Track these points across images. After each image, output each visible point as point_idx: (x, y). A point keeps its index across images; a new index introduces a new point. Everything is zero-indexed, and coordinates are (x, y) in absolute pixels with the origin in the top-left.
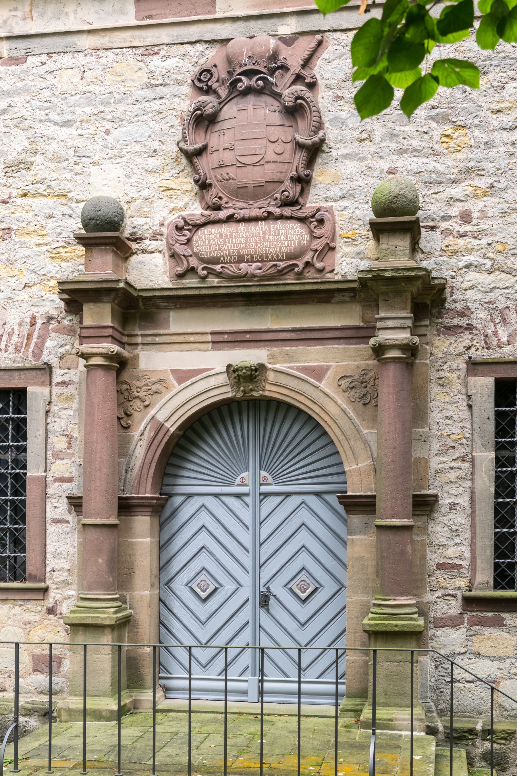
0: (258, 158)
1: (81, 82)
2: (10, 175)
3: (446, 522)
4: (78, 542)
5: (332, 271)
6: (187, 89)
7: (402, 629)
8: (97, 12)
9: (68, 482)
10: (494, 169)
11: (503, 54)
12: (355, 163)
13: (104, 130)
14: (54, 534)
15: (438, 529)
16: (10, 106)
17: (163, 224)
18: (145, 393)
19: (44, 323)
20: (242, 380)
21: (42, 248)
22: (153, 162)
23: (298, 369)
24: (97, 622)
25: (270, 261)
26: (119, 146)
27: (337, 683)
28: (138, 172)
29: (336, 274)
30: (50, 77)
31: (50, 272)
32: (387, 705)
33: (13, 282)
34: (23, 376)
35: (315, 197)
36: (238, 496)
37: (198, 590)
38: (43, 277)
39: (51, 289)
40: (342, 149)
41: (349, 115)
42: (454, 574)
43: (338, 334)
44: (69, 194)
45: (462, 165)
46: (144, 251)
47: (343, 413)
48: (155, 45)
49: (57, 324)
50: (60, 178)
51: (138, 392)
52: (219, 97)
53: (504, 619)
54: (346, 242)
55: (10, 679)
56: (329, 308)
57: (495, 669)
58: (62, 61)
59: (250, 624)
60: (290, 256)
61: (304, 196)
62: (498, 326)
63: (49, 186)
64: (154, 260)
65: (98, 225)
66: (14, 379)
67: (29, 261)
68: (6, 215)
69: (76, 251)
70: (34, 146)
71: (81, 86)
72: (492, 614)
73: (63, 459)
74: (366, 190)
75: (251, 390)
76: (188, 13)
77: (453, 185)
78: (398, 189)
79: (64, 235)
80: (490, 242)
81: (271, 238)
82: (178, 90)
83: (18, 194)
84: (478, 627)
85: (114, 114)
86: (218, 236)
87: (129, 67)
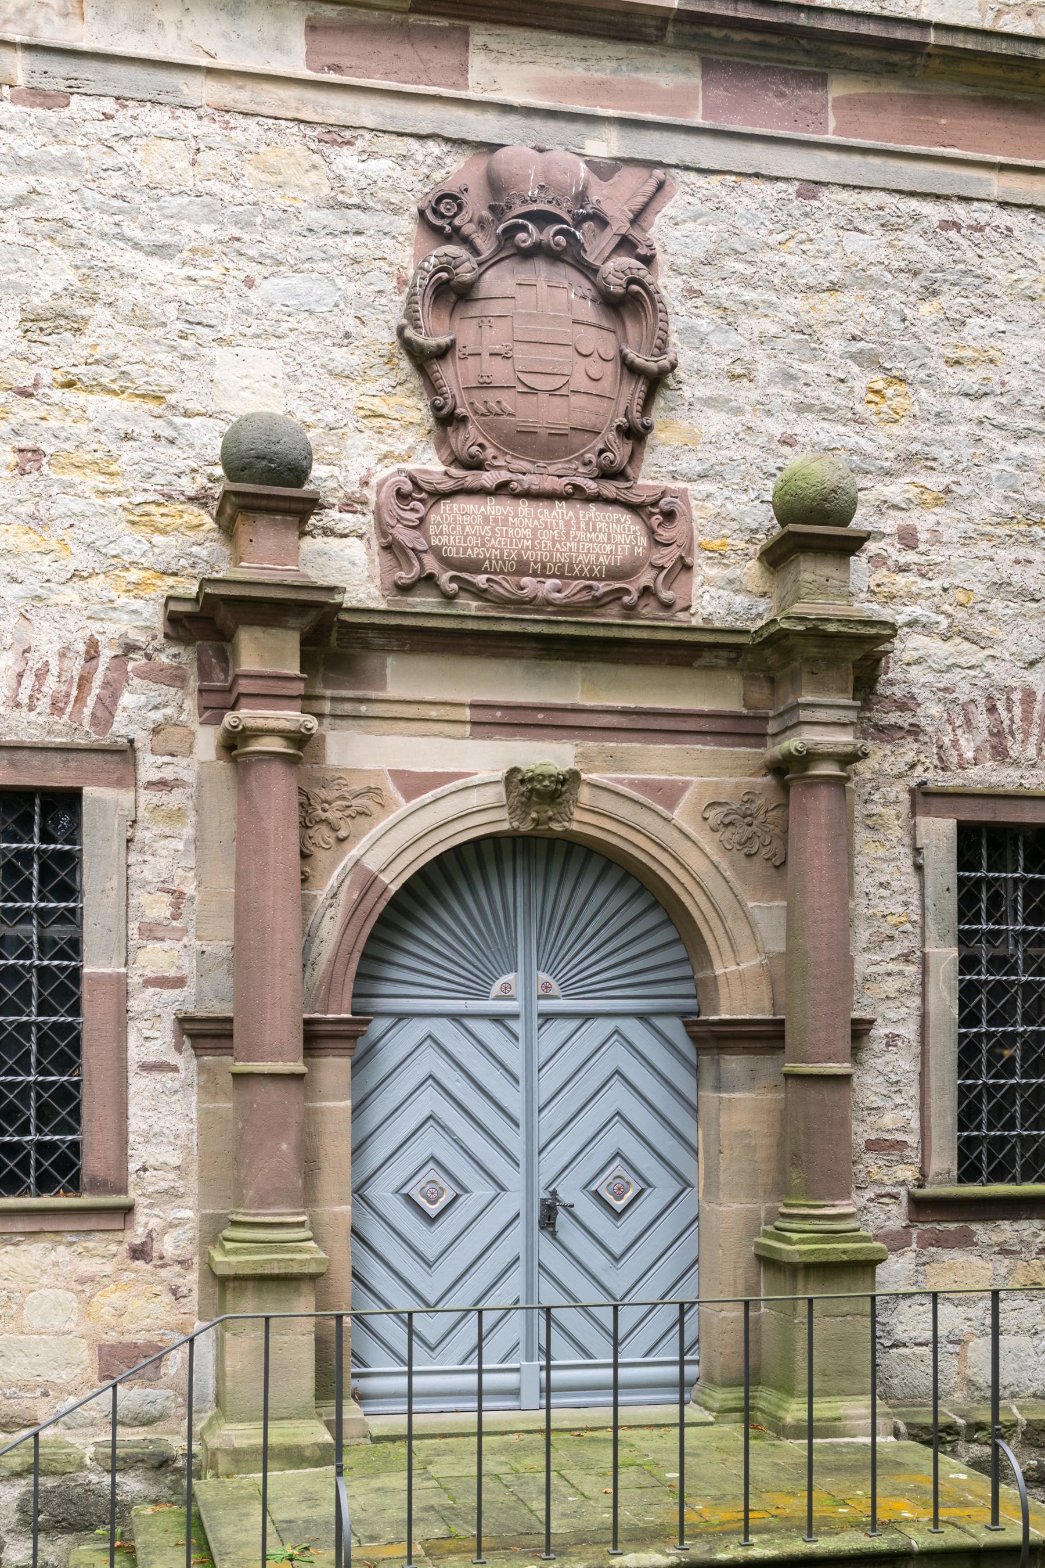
0: (558, 382)
1: (191, 171)
2: (35, 337)
3: (880, 1068)
4: (198, 1110)
5: (687, 609)
6: (408, 225)
7: (853, 1257)
8: (225, 35)
9: (173, 988)
10: (951, 460)
11: (962, 266)
12: (723, 416)
13: (242, 276)
14: (146, 1094)
15: (868, 1079)
16: (34, 191)
17: (366, 483)
18: (339, 814)
19: (116, 657)
20: (534, 799)
21: (110, 500)
22: (342, 357)
23: (631, 784)
24: (289, 1271)
25: (576, 578)
26: (272, 315)
27: (682, 1363)
28: (313, 373)
29: (693, 615)
30: (123, 148)
31: (130, 552)
32: (828, 1394)
33: (45, 564)
34: (73, 764)
35: (654, 469)
36: (498, 1018)
37: (609, 1198)
38: (114, 561)
39: (130, 587)
40: (700, 388)
41: (711, 328)
42: (894, 1158)
43: (704, 725)
44: (168, 396)
45: (901, 447)
46: (328, 532)
47: (714, 870)
48: (347, 127)
49: (144, 661)
50: (147, 360)
51: (325, 811)
52: (475, 251)
53: (973, 1234)
54: (710, 558)
55: (46, 1399)
56: (685, 676)
57: (960, 1320)
58: (148, 119)
59: (522, 1262)
60: (613, 574)
61: (634, 465)
62: (959, 732)
63: (123, 373)
64: (347, 551)
65: (270, 470)
66: (53, 769)
67: (82, 525)
68: (30, 421)
69: (185, 516)
70: (91, 285)
71: (191, 179)
72: (956, 1225)
73: (163, 939)
74: (743, 467)
75: (550, 819)
76: (412, 77)
77: (887, 479)
78: (836, 477)
79: (159, 478)
80: (946, 586)
81: (581, 534)
82: (390, 224)
83: (54, 380)
84: (933, 1249)
85: (263, 248)
86: (479, 519)
87: (292, 160)
